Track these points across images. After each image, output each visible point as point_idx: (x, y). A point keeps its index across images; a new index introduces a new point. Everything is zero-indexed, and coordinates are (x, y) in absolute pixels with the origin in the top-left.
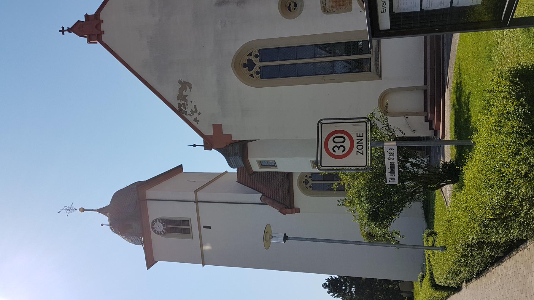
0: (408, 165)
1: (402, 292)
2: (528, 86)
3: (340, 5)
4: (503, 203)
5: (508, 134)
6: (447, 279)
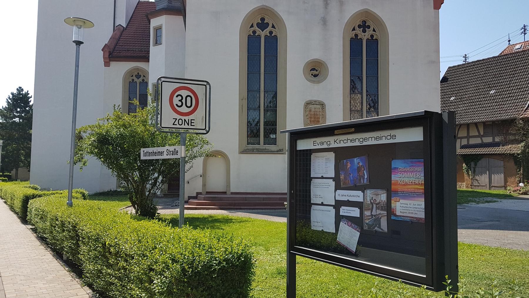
0: (156, 175)
1: (17, 170)
2: (236, 268)
3: (310, 118)
4: (122, 253)
5: (192, 253)
6: (36, 210)
